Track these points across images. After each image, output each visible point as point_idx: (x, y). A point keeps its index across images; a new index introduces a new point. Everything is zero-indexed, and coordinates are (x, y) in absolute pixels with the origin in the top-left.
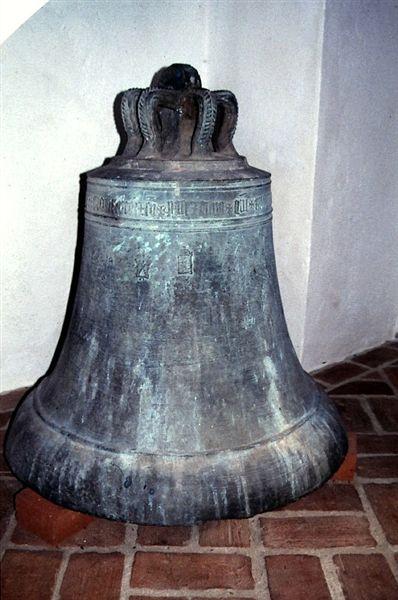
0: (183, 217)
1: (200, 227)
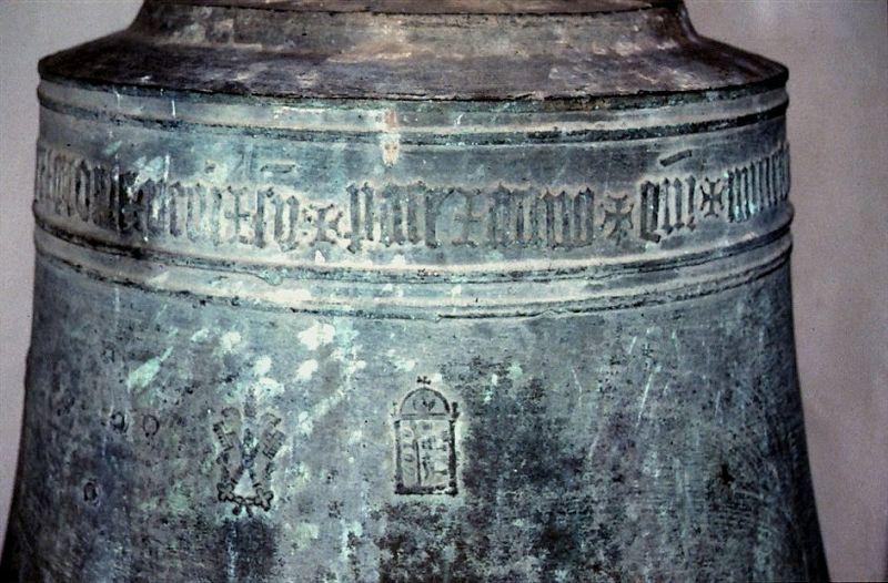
0: (416, 256)
1: (493, 297)
